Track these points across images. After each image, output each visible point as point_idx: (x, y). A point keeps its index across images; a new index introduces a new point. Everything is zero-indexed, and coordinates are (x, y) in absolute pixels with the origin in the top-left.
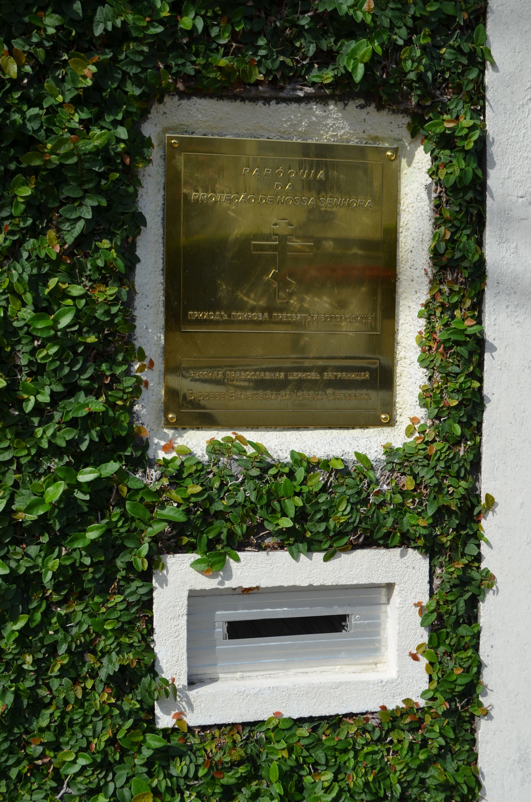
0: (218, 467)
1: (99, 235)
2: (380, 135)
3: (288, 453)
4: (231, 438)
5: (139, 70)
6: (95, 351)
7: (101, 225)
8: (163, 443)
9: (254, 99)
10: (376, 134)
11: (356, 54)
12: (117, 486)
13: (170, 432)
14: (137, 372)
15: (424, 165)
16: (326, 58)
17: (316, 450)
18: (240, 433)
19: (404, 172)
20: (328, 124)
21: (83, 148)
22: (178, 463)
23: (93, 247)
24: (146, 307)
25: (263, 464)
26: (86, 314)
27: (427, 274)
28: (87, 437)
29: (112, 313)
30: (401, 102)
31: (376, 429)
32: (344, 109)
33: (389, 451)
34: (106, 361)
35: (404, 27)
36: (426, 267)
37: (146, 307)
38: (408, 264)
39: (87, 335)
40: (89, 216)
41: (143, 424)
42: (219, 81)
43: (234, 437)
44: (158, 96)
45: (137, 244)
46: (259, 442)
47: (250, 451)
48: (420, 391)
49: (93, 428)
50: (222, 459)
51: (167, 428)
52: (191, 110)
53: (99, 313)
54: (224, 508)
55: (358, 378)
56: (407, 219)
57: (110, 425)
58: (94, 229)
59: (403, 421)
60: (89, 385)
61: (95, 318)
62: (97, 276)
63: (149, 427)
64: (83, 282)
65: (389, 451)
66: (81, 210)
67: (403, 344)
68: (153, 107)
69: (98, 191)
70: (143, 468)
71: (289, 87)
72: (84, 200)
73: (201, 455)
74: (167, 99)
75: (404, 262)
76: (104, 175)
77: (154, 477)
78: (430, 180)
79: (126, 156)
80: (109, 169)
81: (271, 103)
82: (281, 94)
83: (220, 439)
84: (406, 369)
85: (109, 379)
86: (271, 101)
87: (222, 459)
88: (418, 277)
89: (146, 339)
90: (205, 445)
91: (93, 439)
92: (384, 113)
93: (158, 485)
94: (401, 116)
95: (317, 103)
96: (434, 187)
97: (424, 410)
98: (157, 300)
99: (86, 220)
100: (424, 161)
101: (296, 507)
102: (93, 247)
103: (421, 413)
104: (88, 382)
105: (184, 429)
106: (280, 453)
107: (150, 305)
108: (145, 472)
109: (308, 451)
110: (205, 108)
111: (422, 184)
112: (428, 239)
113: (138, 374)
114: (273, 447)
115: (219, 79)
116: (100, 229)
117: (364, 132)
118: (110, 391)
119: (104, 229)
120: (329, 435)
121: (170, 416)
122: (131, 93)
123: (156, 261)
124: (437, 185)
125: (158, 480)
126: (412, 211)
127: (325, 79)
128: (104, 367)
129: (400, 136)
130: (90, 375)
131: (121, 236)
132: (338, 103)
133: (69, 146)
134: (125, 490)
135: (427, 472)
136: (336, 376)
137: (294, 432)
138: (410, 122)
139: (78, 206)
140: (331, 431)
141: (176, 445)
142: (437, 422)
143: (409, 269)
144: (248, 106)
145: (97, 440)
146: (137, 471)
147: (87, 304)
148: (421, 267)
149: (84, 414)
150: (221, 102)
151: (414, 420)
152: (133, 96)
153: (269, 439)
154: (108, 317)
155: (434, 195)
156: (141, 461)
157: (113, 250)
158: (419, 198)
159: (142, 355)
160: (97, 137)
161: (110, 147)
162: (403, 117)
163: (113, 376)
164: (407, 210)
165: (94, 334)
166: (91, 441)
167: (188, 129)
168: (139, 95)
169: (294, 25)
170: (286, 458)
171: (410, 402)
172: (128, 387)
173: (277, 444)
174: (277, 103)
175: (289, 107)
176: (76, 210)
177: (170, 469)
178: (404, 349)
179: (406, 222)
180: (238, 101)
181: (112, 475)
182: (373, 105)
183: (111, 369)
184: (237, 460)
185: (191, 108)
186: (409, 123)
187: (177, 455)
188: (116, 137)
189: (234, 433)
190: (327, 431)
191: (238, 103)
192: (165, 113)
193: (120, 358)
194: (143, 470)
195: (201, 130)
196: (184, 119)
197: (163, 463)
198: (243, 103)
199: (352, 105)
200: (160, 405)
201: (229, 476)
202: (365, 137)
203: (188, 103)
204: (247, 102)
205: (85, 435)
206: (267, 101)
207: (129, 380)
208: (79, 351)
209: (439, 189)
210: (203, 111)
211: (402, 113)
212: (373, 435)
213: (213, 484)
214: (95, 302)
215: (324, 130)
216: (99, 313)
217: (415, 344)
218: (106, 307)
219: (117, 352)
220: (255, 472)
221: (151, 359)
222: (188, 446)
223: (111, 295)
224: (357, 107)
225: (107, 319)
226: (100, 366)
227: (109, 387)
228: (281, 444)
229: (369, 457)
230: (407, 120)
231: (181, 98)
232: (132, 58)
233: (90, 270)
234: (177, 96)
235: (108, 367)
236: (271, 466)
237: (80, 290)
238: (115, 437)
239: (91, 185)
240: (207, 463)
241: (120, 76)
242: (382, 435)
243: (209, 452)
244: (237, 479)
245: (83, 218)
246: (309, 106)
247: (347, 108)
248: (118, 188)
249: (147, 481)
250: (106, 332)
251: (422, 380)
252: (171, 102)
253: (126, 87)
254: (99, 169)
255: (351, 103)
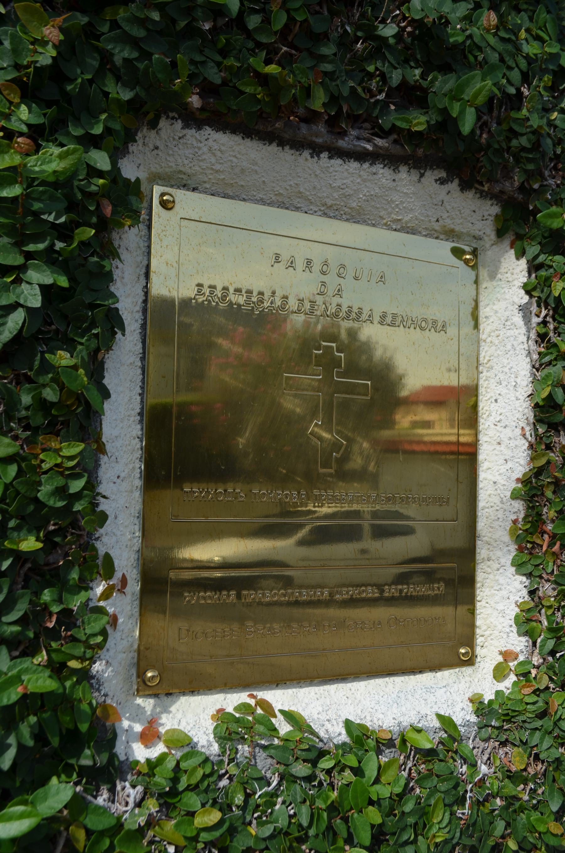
0: (238, 765)
1: (46, 342)
2: (457, 228)
3: (341, 725)
4: (249, 705)
5: (135, 55)
6: (29, 565)
7: (51, 324)
8: (138, 728)
9: (298, 145)
10: (452, 226)
11: (463, 92)
12: (67, 829)
13: (147, 704)
14: (99, 600)
15: (515, 276)
16: (412, 96)
17: (381, 716)
18: (262, 695)
19: (484, 286)
20: (393, 202)
21: (37, 169)
22: (170, 764)
23: (37, 363)
24: (115, 479)
25: (307, 748)
26: (18, 493)
27: (524, 435)
28: (12, 740)
29: (72, 491)
30: (497, 181)
31: (452, 671)
32: (419, 181)
33: (481, 708)
34: (49, 585)
35: (516, 69)
36: (522, 424)
37: (115, 479)
38: (491, 418)
39: (15, 534)
40: (36, 302)
41: (106, 695)
42: (259, 101)
43: (252, 702)
44: (151, 116)
45: (106, 366)
46: (293, 708)
47: (284, 728)
48: (517, 610)
49: (22, 719)
50: (240, 747)
51: (141, 697)
52: (199, 148)
53: (44, 492)
54: (255, 843)
55: (429, 592)
56: (489, 353)
57: (55, 710)
58: (39, 331)
59: (488, 654)
60: (19, 633)
61: (36, 500)
62: (39, 420)
63: (115, 699)
64: (12, 430)
65: (481, 708)
66: (18, 291)
67: (484, 539)
68: (140, 135)
69: (50, 258)
70: (108, 783)
71: (354, 133)
72: (25, 272)
73: (205, 743)
74: (163, 123)
75: (484, 416)
76: (64, 231)
77: (131, 801)
78: (526, 298)
79: (105, 202)
80: (72, 222)
81: (322, 155)
82: (342, 143)
83: (230, 709)
84: (491, 576)
85: (54, 619)
86: (321, 152)
87: (240, 747)
88: (510, 438)
89: (114, 539)
90: (210, 725)
91: (23, 741)
92: (470, 194)
93: (140, 815)
94: (490, 203)
95: (385, 166)
96: (534, 308)
97: (524, 639)
98: (131, 466)
99: (30, 311)
100: (515, 271)
101: (373, 826)
102: (37, 363)
103: (519, 644)
104: (16, 628)
105: (168, 694)
106: (328, 726)
107: (123, 475)
108: (112, 791)
109: (368, 718)
110: (223, 148)
111: (514, 303)
112: (525, 383)
113: (102, 604)
114: (316, 716)
115: (259, 96)
116: (49, 332)
117: (438, 221)
118: (56, 640)
119: (57, 331)
120: (390, 686)
121: (149, 674)
122: (115, 96)
123: (131, 398)
124: (539, 306)
125: (139, 805)
126: (496, 342)
127: (416, 125)
128: (47, 596)
129: (481, 233)
130: (21, 613)
131: (87, 348)
132: (412, 170)
133: (12, 159)
134: (81, 835)
135: (542, 739)
136: (401, 591)
137: (341, 686)
138: (499, 213)
139: (13, 282)
140: (392, 679)
141: (162, 730)
142: (550, 659)
143: (493, 426)
144: (287, 155)
145: (30, 743)
146: (98, 790)
147: (20, 473)
148: (514, 424)
149: (14, 698)
150: (248, 142)
151: (507, 655)
152: (118, 101)
153: (306, 701)
154: (61, 499)
155: (535, 320)
156: (111, 772)
157: (81, 371)
158: (508, 323)
159: (108, 567)
160: (51, 161)
161: (76, 183)
162: (492, 205)
163: (66, 613)
164: (489, 340)
165: (30, 532)
166: (21, 747)
167: (189, 182)
168: (128, 102)
169: (371, 35)
170: (340, 734)
171: (500, 627)
172: (95, 635)
173: (320, 709)
174: (330, 158)
175: (346, 167)
176: (8, 290)
177: (157, 779)
178: (487, 546)
179: (487, 358)
180: (275, 144)
181: (60, 811)
182: (456, 181)
183: (60, 601)
184: (264, 748)
185: (199, 145)
186: (497, 216)
187: (166, 750)
188: (88, 165)
189: (252, 696)
190: (387, 679)
191: (273, 148)
192: (157, 148)
193: (74, 575)
194: (109, 786)
195: (208, 186)
196: (186, 162)
197: (145, 770)
198: (280, 148)
199: (431, 176)
200: (131, 655)
201: (256, 779)
202: (437, 228)
203: (197, 135)
204: (287, 148)
205: (7, 737)
206: (316, 150)
207: (95, 620)
208: (4, 567)
209: (544, 313)
210: (219, 154)
211: (491, 199)
212: (451, 681)
213: (233, 798)
214: (36, 469)
215: (386, 210)
216: (44, 492)
217: (507, 538)
218: (60, 481)
219: (69, 565)
220: (301, 769)
221: (124, 575)
222: (181, 728)
223: (71, 458)
224: (436, 181)
225: (60, 504)
226: (38, 594)
227: (54, 634)
228: (327, 708)
229: (454, 718)
230: (496, 210)
231: (186, 126)
232: (127, 29)
233: (27, 408)
234: (179, 121)
235: (56, 597)
236: (322, 754)
237: (9, 445)
238: (64, 732)
239: (41, 246)
240: (217, 758)
241: (96, 64)
242: (463, 681)
243: (220, 738)
244: (269, 784)
245: (22, 306)
246: (374, 169)
247: (423, 180)
248: (86, 259)
249: (118, 808)
250: (52, 528)
251: (520, 594)
252: (170, 129)
253: (105, 85)
254: (56, 218)
255: (428, 173)
